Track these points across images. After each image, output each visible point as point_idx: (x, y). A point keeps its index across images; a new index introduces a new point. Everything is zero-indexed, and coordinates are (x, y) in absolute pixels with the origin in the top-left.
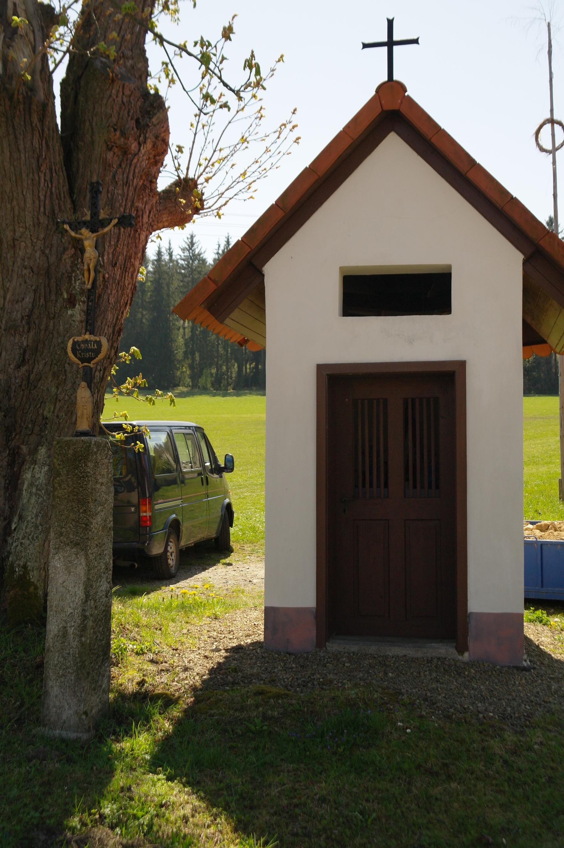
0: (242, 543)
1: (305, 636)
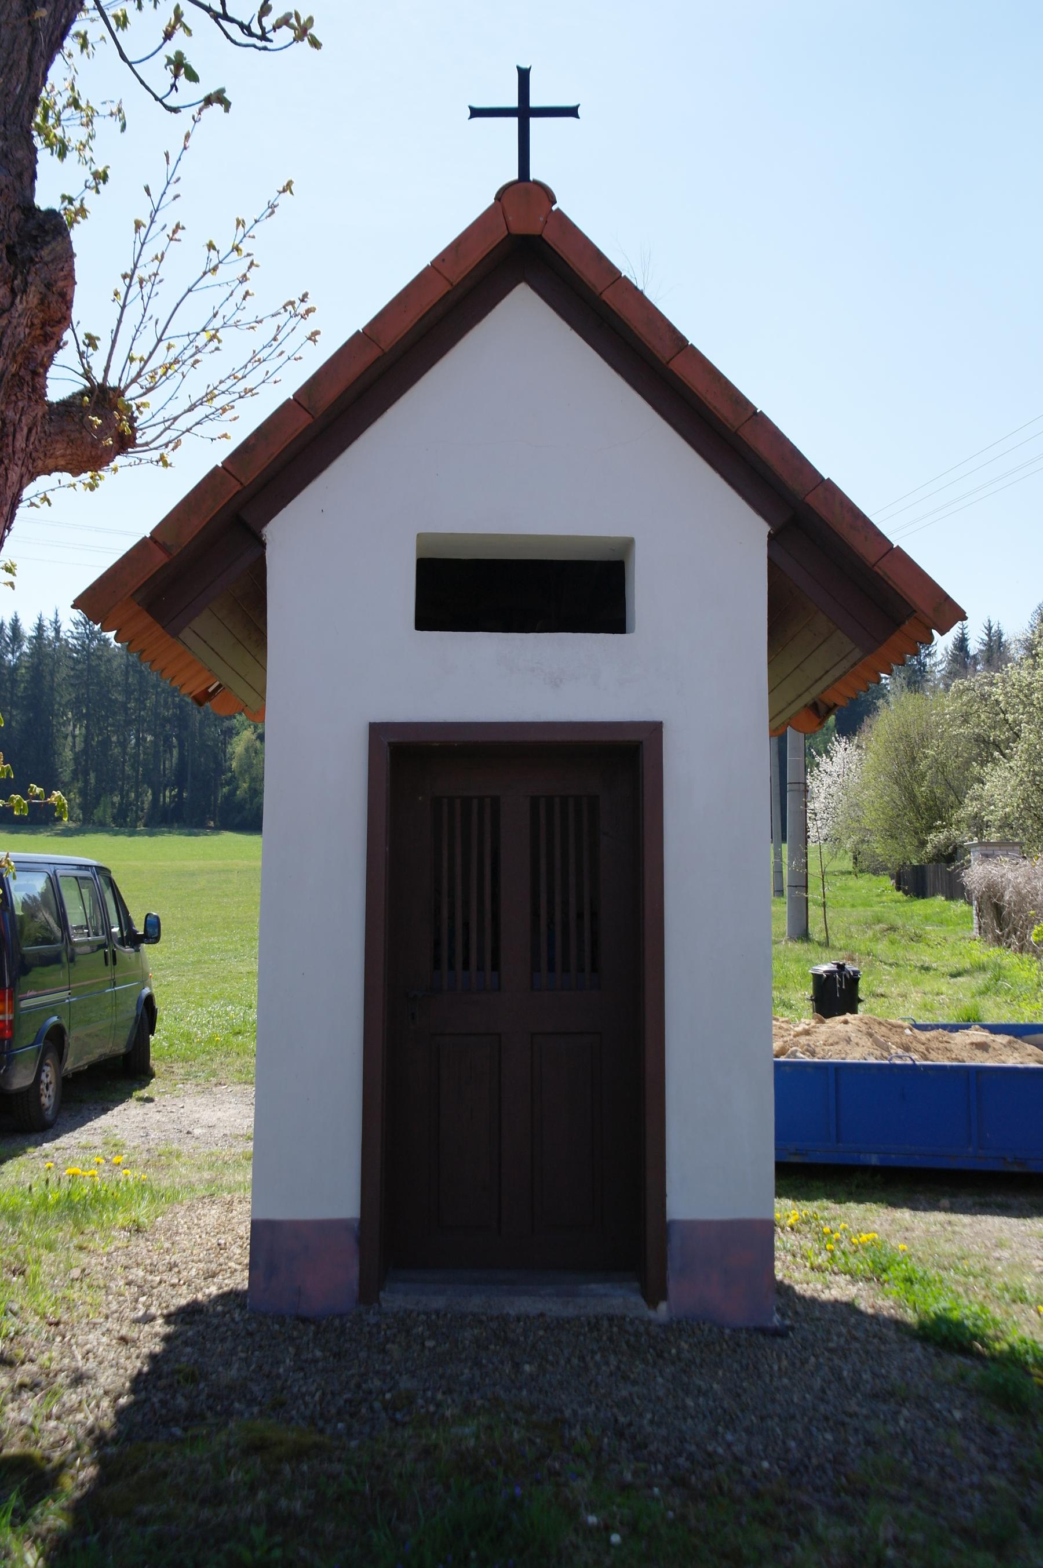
0: (170, 1060)
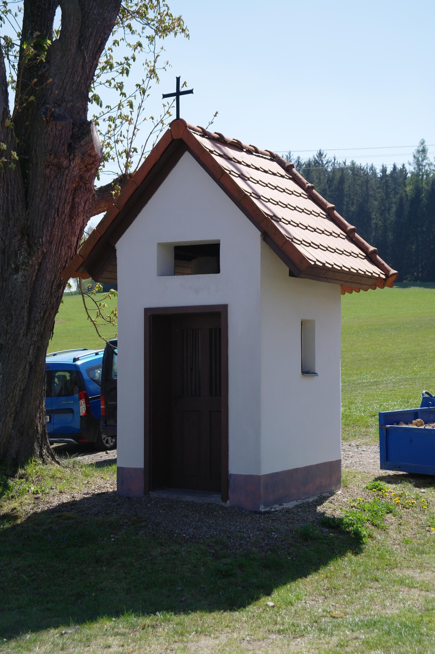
1: (137, 487)
